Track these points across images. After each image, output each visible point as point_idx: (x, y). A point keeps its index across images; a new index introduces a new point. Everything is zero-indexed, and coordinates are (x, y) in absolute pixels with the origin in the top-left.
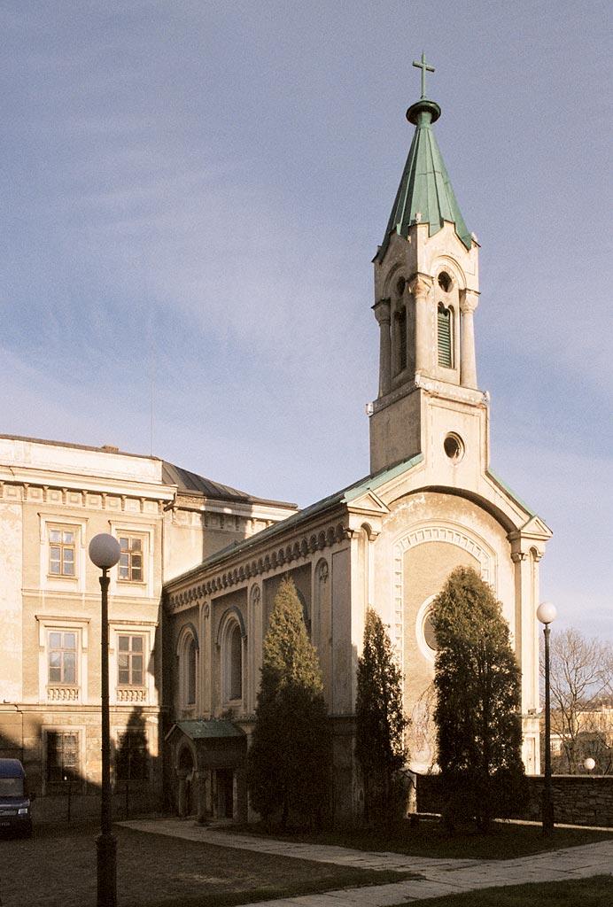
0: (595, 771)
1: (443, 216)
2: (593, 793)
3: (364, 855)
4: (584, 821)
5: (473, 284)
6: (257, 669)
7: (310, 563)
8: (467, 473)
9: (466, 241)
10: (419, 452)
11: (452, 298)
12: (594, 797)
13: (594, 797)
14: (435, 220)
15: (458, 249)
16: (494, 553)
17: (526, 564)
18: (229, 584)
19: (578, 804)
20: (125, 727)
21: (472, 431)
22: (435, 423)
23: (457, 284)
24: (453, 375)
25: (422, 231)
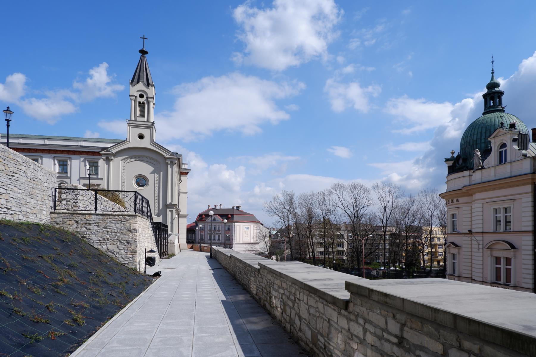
11: (142, 100)
15: (144, 88)
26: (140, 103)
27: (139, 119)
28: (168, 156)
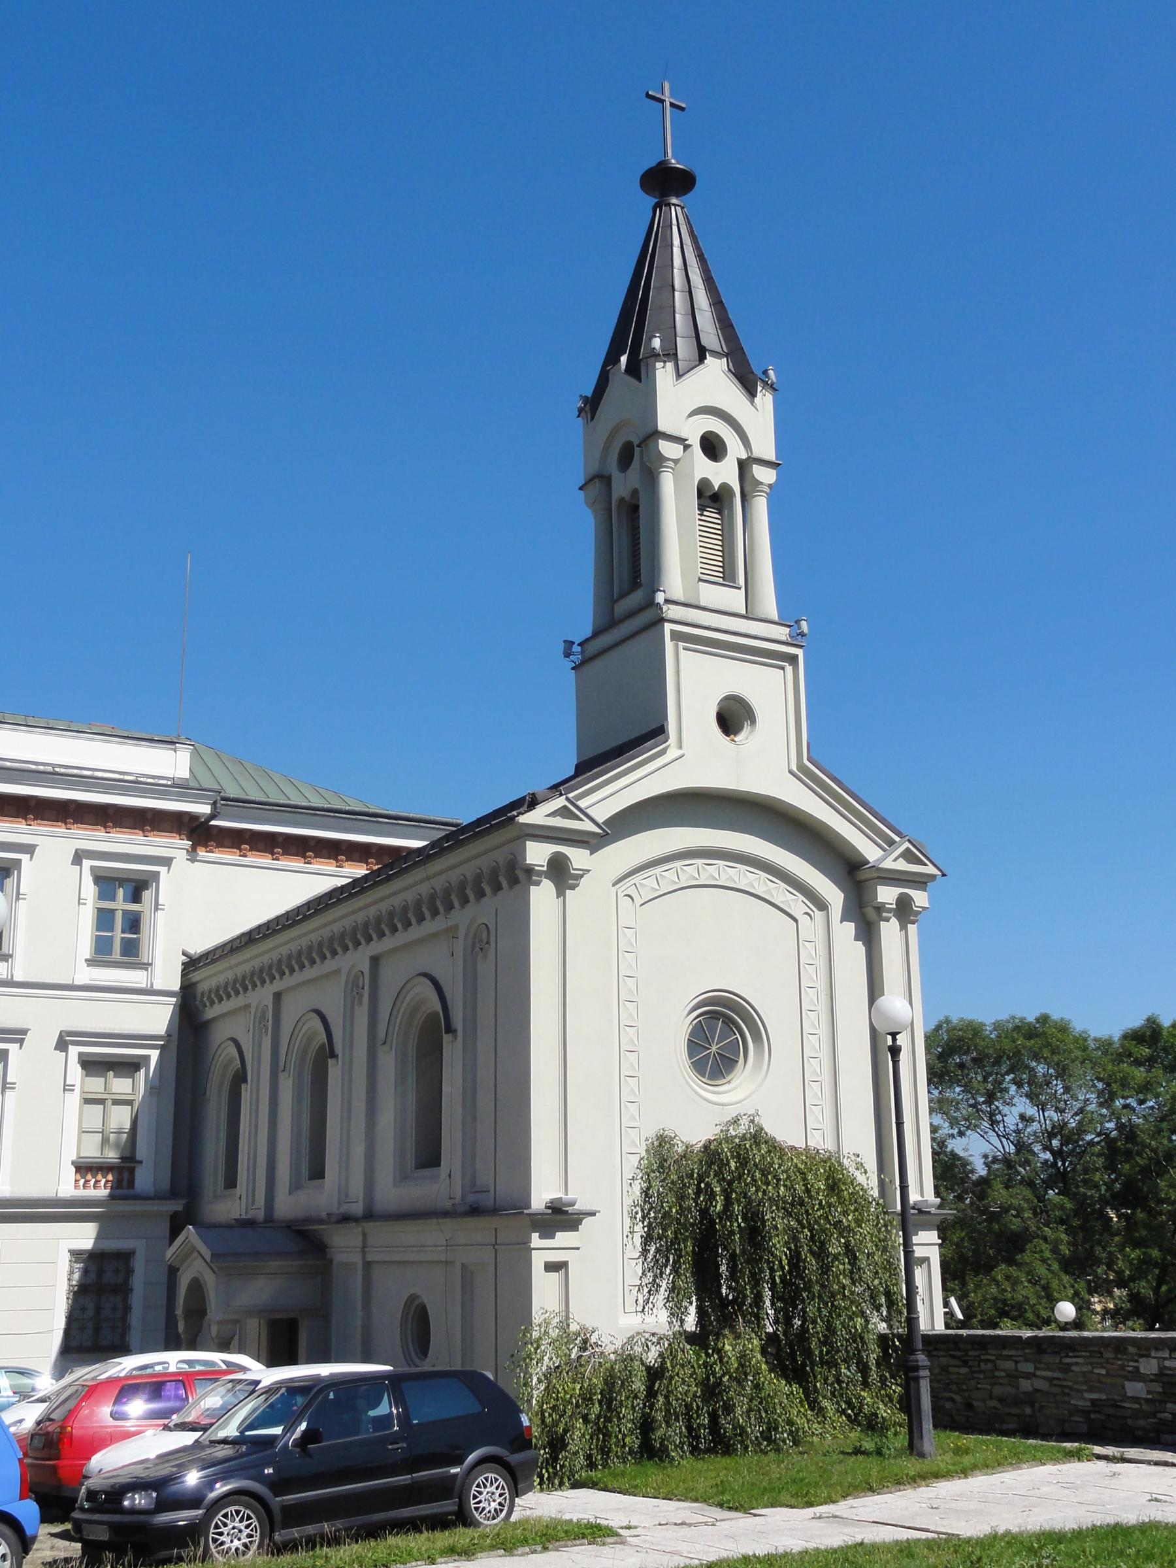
0: (1078, 1324)
1: (704, 342)
2: (1029, 1367)
3: (760, 1548)
4: (1011, 1426)
5: (765, 445)
6: (460, 1033)
7: (457, 926)
8: (764, 764)
9: (747, 380)
10: (658, 732)
11: (724, 473)
12: (1028, 1376)
13: (1028, 1376)
14: (684, 348)
15: (730, 395)
16: (821, 904)
17: (889, 930)
18: (297, 968)
19: (998, 1390)
20: (92, 1241)
21: (770, 691)
22: (695, 684)
23: (735, 450)
24: (734, 599)
25: (663, 373)
26: (703, 488)
27: (713, 595)
28: (889, 864)
